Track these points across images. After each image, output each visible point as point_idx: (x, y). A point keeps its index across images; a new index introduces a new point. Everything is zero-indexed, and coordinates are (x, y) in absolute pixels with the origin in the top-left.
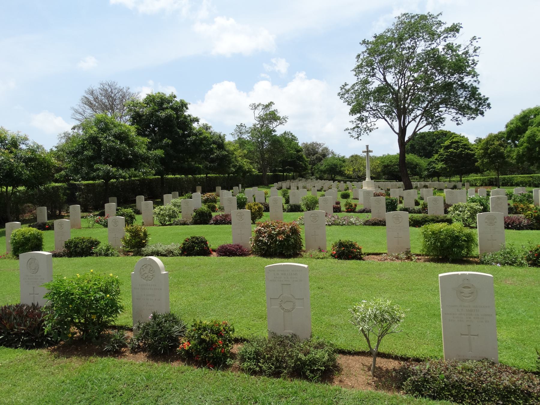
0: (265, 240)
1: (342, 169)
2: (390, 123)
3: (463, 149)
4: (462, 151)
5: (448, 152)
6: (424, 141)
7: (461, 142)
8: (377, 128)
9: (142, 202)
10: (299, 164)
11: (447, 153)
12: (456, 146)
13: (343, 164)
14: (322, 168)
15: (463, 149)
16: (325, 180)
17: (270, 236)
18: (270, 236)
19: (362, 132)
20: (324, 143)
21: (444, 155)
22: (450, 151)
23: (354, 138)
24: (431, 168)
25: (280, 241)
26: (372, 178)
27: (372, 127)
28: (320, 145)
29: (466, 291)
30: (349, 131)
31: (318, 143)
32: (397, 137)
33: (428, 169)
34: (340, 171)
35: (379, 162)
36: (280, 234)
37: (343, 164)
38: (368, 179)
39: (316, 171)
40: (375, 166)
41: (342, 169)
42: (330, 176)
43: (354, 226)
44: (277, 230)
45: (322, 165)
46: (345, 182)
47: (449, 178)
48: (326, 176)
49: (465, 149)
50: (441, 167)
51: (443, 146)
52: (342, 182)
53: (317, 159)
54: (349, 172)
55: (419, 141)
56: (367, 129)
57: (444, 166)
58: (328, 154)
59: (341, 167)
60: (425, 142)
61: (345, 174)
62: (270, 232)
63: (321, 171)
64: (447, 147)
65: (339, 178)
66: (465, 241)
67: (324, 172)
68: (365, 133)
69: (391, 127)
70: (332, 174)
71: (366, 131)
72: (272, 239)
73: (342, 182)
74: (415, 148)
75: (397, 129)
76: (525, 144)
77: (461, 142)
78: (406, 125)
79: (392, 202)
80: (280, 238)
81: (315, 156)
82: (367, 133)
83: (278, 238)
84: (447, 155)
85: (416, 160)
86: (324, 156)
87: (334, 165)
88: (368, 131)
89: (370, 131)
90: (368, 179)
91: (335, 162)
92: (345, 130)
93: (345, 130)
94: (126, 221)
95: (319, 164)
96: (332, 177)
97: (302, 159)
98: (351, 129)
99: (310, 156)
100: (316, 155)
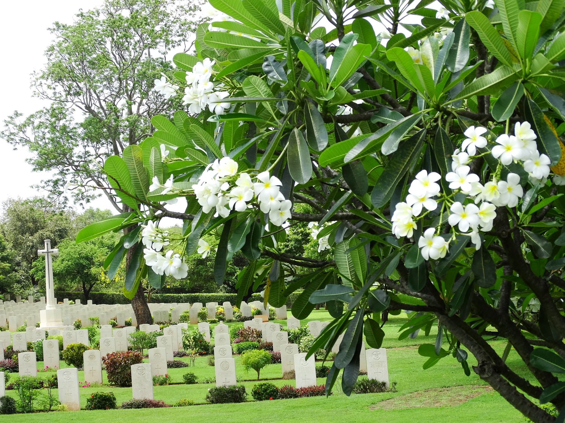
11: (295, 236)
81: (37, 235)
100: (40, 232)
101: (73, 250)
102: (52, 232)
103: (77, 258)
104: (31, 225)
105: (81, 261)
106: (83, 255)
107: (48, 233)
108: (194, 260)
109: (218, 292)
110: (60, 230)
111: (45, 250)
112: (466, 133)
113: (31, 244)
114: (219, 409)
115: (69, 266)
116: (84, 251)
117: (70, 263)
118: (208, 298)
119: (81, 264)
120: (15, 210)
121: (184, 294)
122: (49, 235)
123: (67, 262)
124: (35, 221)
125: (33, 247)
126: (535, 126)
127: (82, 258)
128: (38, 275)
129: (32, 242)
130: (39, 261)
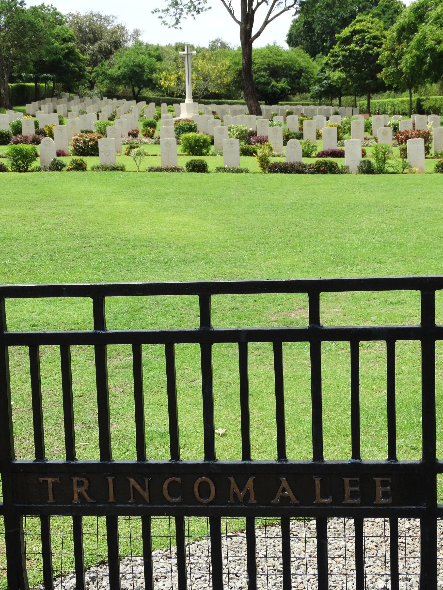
0: (81, 145)
1: (155, 75)
2: (228, 5)
3: (371, 46)
4: (368, 49)
5: (346, 51)
6: (332, 16)
7: (368, 32)
8: (210, 8)
9: (164, 105)
10: (68, 66)
11: (344, 53)
12: (360, 40)
13: (158, 65)
14: (114, 71)
15: (371, 46)
16: (119, 98)
17: (85, 142)
18: (85, 142)
19: (184, 14)
20: (115, 14)
21: (339, 56)
22: (349, 49)
23: (167, 26)
24: (325, 79)
25: (91, 145)
26: (195, 98)
27: (201, 6)
28: (107, 19)
29: (168, 144)
30: (160, 14)
31: (103, 15)
32: (237, 29)
33: (320, 81)
34: (150, 80)
35: (228, 63)
36: (91, 141)
37: (158, 65)
38: (189, 100)
39: (101, 78)
40: (221, 72)
41: (155, 75)
42: (129, 90)
43: (146, 145)
44: (89, 138)
45: (114, 64)
46: (158, 104)
47: (407, 93)
48: (121, 88)
49: (375, 45)
50: (340, 78)
51: (339, 38)
52: (153, 104)
53: (100, 51)
54: (167, 83)
55: (322, 15)
56: (192, 9)
57: (343, 75)
58: (125, 41)
59: (153, 70)
60: (334, 17)
61: (161, 87)
62: (84, 140)
63: (112, 79)
64: (347, 41)
65: (150, 94)
66: (202, 142)
67: (116, 80)
68: (190, 14)
69: (230, 11)
70: (133, 86)
71: (190, 11)
72: (86, 144)
73: (153, 104)
74: (314, 29)
75: (238, 15)
76: (414, 51)
77: (368, 32)
78: (253, 9)
79: (190, 127)
80: (92, 143)
81: (96, 45)
82: (193, 15)
83: (90, 143)
84: (344, 56)
85: (300, 60)
86: (117, 44)
87: (139, 66)
88: (195, 13)
89: (198, 12)
90: (189, 100)
91: (140, 59)
92: (152, 12)
93: (152, 12)
94: (156, 105)
95: (106, 63)
96: (133, 91)
97: (74, 55)
98: (163, 11)
99: (85, 44)
100: (99, 42)
101: (127, 59)
102: (108, 43)
103: (132, 66)
104: (91, 36)
105: (135, 68)
106: (136, 63)
107: (105, 44)
108: (237, 70)
109: (240, 100)
110: (115, 42)
111: (185, 52)
112: (434, 84)
113: (92, 52)
114: (73, 327)
115: (125, 72)
116: (137, 60)
117: (126, 69)
118: (53, 165)
119: (135, 71)
120: (77, 23)
121: (212, 100)
122: (107, 46)
123: (123, 68)
124: (94, 34)
125: (93, 55)
126: (145, 485)
127: (136, 66)
128: (99, 78)
129: (93, 50)
130: (99, 67)
